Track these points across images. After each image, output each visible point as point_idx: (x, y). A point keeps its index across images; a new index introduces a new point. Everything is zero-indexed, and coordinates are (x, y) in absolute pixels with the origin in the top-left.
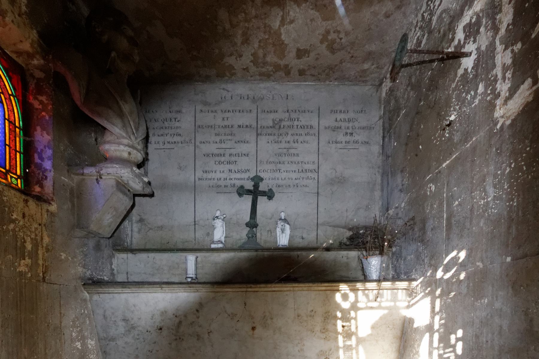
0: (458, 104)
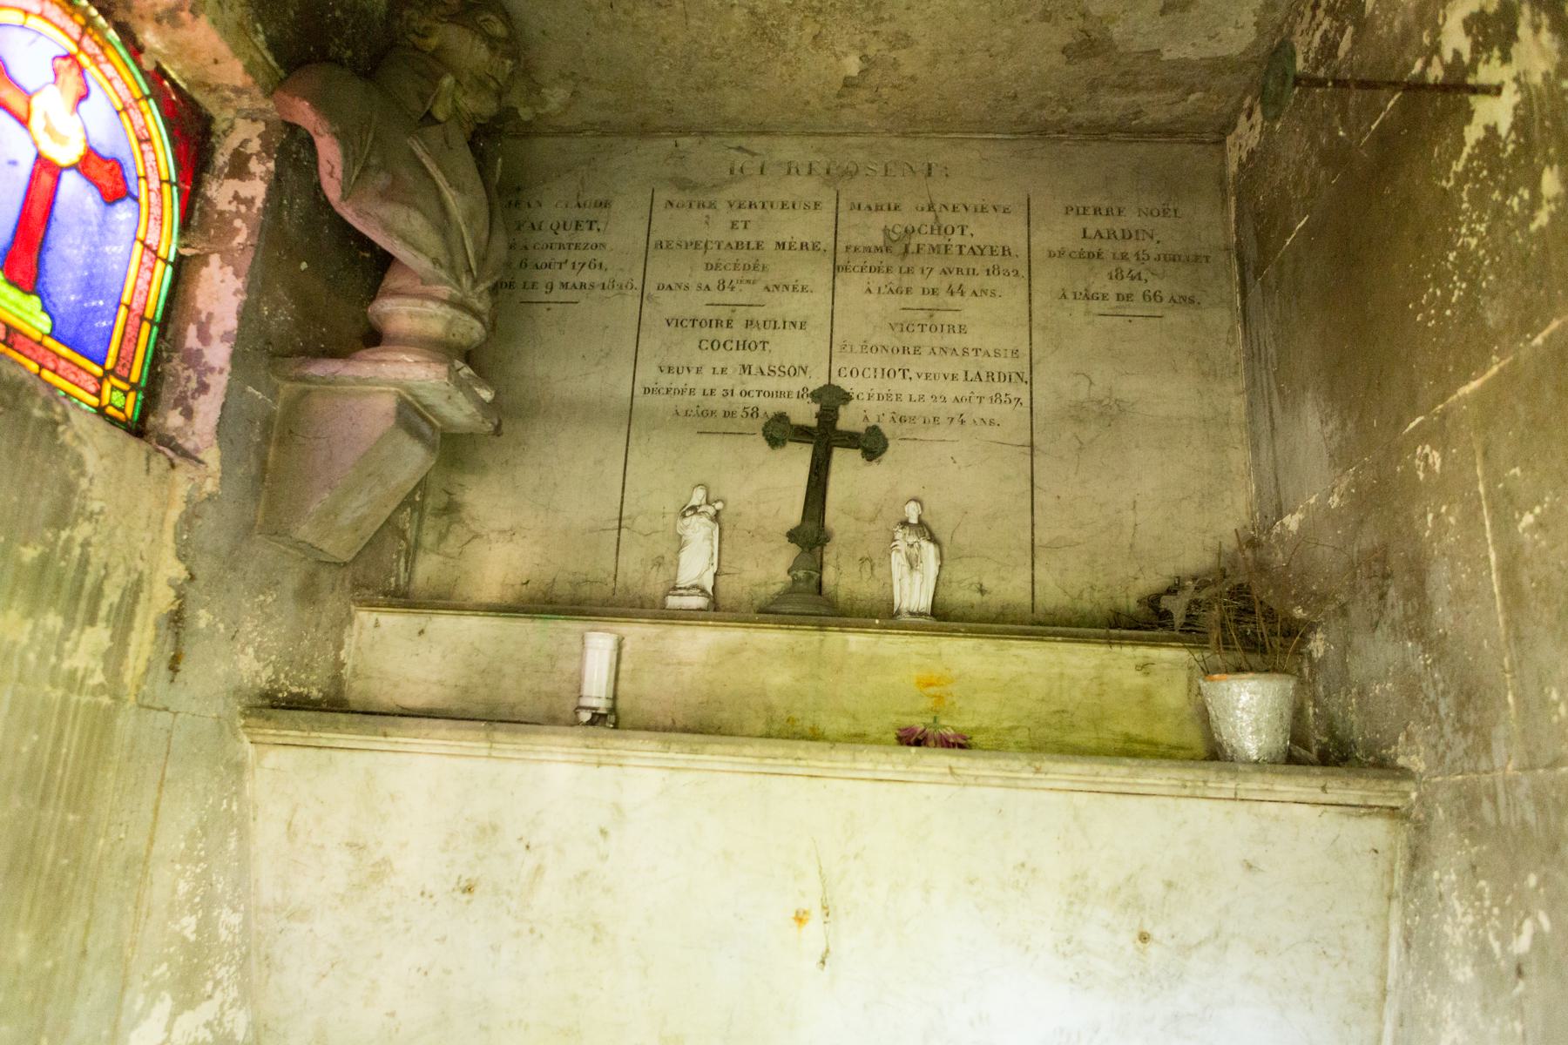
0: (1480, 220)
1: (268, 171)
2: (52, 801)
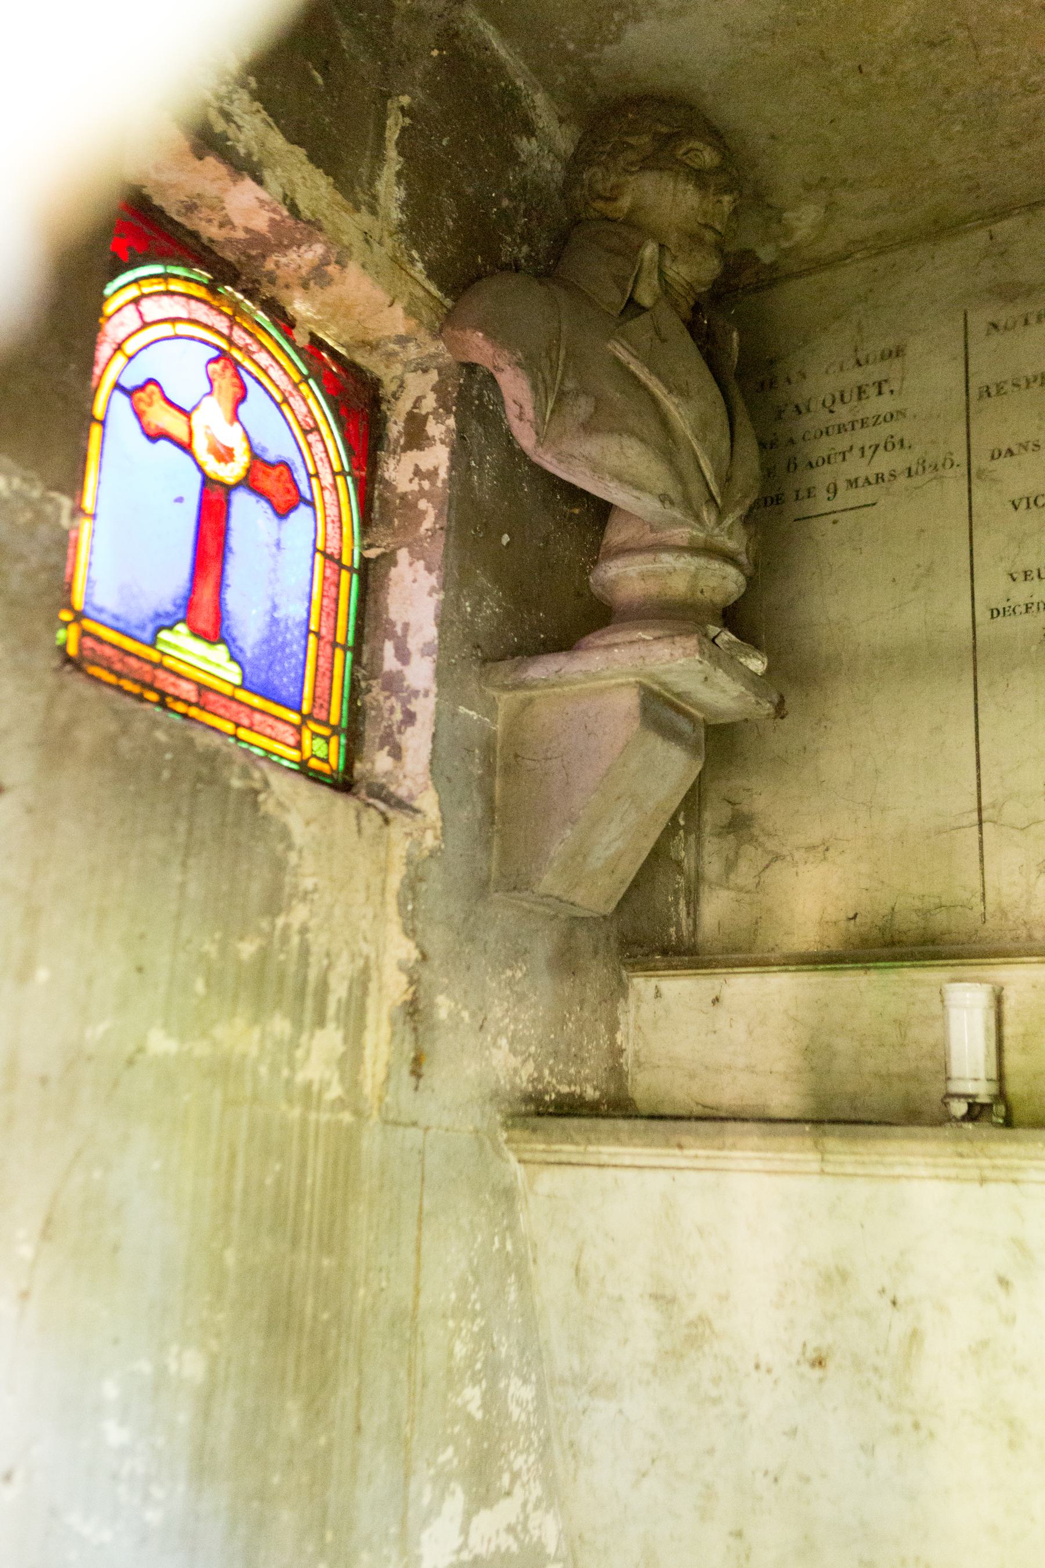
1: (448, 430)
2: (304, 1242)
